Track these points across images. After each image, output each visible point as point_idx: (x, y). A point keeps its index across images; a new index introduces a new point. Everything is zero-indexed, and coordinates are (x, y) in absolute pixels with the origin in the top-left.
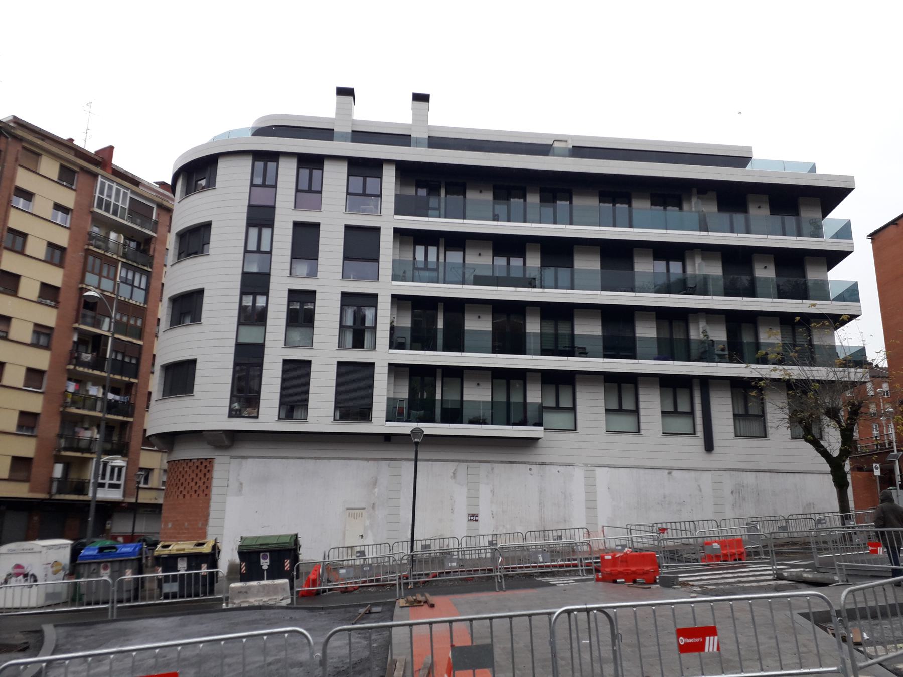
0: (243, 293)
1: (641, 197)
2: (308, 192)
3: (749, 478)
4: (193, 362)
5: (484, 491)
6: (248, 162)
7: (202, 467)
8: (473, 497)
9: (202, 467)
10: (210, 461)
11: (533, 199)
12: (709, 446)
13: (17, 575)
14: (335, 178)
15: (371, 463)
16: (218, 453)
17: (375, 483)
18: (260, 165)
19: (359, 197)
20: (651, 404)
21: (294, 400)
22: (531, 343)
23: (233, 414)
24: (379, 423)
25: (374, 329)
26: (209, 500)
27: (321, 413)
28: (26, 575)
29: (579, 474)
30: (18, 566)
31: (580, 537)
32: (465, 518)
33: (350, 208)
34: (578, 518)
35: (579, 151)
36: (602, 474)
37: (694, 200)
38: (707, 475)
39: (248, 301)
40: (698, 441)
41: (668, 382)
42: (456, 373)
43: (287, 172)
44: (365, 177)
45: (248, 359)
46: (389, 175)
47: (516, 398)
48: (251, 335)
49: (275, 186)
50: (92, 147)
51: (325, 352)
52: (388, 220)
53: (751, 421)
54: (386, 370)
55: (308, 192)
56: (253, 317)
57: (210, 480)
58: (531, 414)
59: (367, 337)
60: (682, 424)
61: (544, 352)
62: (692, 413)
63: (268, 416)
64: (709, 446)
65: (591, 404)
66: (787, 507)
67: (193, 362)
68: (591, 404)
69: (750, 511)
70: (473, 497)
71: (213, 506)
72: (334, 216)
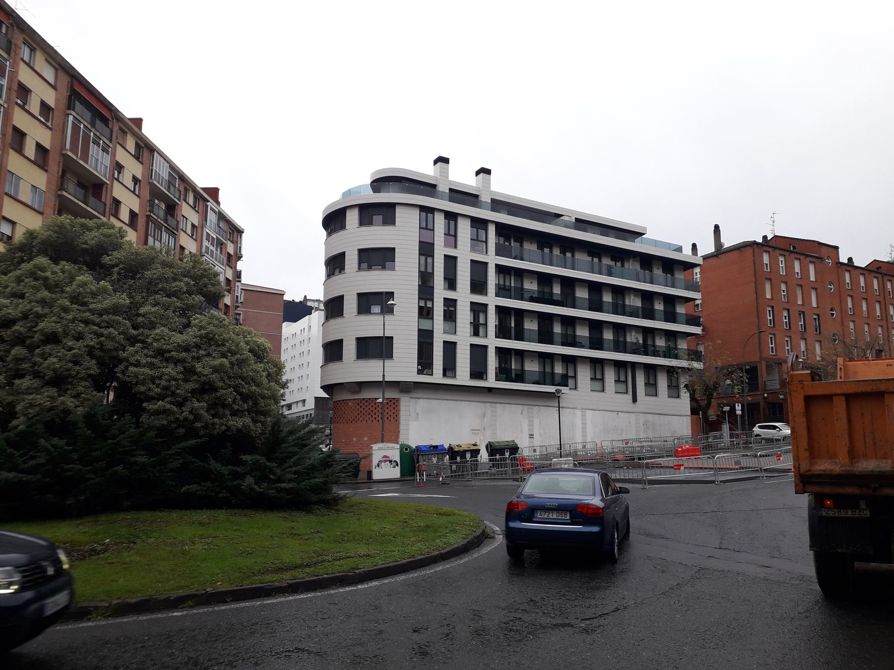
0: (420, 298)
1: (606, 256)
2: (452, 236)
3: (650, 417)
4: (341, 341)
5: (536, 422)
6: (417, 212)
7: (392, 403)
8: (531, 425)
9: (392, 403)
10: (398, 400)
11: (556, 252)
12: (635, 400)
13: (385, 461)
14: (464, 229)
15: (482, 404)
16: (403, 395)
17: (484, 416)
18: (423, 214)
19: (478, 242)
20: (610, 376)
21: (450, 367)
22: (557, 338)
23: (420, 372)
24: (491, 381)
25: (486, 325)
26: (399, 423)
27: (463, 376)
28: (390, 461)
29: (579, 413)
30: (385, 457)
31: (580, 447)
32: (528, 437)
33: (473, 249)
34: (579, 439)
35: (582, 223)
36: (588, 413)
37: (631, 261)
38: (633, 415)
39: (429, 305)
40: (629, 397)
41: (619, 365)
42: (521, 354)
43: (440, 221)
44: (478, 229)
45: (425, 340)
46: (492, 229)
47: (548, 370)
48: (426, 325)
49: (433, 230)
50: (201, 181)
51: (464, 339)
52: (493, 260)
53: (652, 387)
54: (494, 350)
55: (452, 236)
56: (425, 313)
57: (398, 411)
58: (558, 379)
59: (481, 330)
60: (622, 387)
61: (563, 344)
62: (626, 382)
63: (437, 377)
64: (635, 400)
65: (584, 374)
66: (666, 433)
67: (341, 341)
68: (584, 374)
69: (651, 435)
70: (531, 425)
71: (402, 427)
72: (465, 255)
